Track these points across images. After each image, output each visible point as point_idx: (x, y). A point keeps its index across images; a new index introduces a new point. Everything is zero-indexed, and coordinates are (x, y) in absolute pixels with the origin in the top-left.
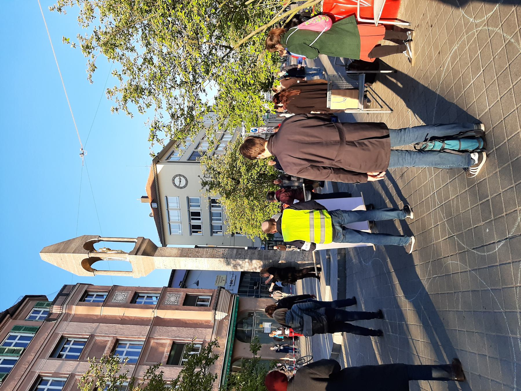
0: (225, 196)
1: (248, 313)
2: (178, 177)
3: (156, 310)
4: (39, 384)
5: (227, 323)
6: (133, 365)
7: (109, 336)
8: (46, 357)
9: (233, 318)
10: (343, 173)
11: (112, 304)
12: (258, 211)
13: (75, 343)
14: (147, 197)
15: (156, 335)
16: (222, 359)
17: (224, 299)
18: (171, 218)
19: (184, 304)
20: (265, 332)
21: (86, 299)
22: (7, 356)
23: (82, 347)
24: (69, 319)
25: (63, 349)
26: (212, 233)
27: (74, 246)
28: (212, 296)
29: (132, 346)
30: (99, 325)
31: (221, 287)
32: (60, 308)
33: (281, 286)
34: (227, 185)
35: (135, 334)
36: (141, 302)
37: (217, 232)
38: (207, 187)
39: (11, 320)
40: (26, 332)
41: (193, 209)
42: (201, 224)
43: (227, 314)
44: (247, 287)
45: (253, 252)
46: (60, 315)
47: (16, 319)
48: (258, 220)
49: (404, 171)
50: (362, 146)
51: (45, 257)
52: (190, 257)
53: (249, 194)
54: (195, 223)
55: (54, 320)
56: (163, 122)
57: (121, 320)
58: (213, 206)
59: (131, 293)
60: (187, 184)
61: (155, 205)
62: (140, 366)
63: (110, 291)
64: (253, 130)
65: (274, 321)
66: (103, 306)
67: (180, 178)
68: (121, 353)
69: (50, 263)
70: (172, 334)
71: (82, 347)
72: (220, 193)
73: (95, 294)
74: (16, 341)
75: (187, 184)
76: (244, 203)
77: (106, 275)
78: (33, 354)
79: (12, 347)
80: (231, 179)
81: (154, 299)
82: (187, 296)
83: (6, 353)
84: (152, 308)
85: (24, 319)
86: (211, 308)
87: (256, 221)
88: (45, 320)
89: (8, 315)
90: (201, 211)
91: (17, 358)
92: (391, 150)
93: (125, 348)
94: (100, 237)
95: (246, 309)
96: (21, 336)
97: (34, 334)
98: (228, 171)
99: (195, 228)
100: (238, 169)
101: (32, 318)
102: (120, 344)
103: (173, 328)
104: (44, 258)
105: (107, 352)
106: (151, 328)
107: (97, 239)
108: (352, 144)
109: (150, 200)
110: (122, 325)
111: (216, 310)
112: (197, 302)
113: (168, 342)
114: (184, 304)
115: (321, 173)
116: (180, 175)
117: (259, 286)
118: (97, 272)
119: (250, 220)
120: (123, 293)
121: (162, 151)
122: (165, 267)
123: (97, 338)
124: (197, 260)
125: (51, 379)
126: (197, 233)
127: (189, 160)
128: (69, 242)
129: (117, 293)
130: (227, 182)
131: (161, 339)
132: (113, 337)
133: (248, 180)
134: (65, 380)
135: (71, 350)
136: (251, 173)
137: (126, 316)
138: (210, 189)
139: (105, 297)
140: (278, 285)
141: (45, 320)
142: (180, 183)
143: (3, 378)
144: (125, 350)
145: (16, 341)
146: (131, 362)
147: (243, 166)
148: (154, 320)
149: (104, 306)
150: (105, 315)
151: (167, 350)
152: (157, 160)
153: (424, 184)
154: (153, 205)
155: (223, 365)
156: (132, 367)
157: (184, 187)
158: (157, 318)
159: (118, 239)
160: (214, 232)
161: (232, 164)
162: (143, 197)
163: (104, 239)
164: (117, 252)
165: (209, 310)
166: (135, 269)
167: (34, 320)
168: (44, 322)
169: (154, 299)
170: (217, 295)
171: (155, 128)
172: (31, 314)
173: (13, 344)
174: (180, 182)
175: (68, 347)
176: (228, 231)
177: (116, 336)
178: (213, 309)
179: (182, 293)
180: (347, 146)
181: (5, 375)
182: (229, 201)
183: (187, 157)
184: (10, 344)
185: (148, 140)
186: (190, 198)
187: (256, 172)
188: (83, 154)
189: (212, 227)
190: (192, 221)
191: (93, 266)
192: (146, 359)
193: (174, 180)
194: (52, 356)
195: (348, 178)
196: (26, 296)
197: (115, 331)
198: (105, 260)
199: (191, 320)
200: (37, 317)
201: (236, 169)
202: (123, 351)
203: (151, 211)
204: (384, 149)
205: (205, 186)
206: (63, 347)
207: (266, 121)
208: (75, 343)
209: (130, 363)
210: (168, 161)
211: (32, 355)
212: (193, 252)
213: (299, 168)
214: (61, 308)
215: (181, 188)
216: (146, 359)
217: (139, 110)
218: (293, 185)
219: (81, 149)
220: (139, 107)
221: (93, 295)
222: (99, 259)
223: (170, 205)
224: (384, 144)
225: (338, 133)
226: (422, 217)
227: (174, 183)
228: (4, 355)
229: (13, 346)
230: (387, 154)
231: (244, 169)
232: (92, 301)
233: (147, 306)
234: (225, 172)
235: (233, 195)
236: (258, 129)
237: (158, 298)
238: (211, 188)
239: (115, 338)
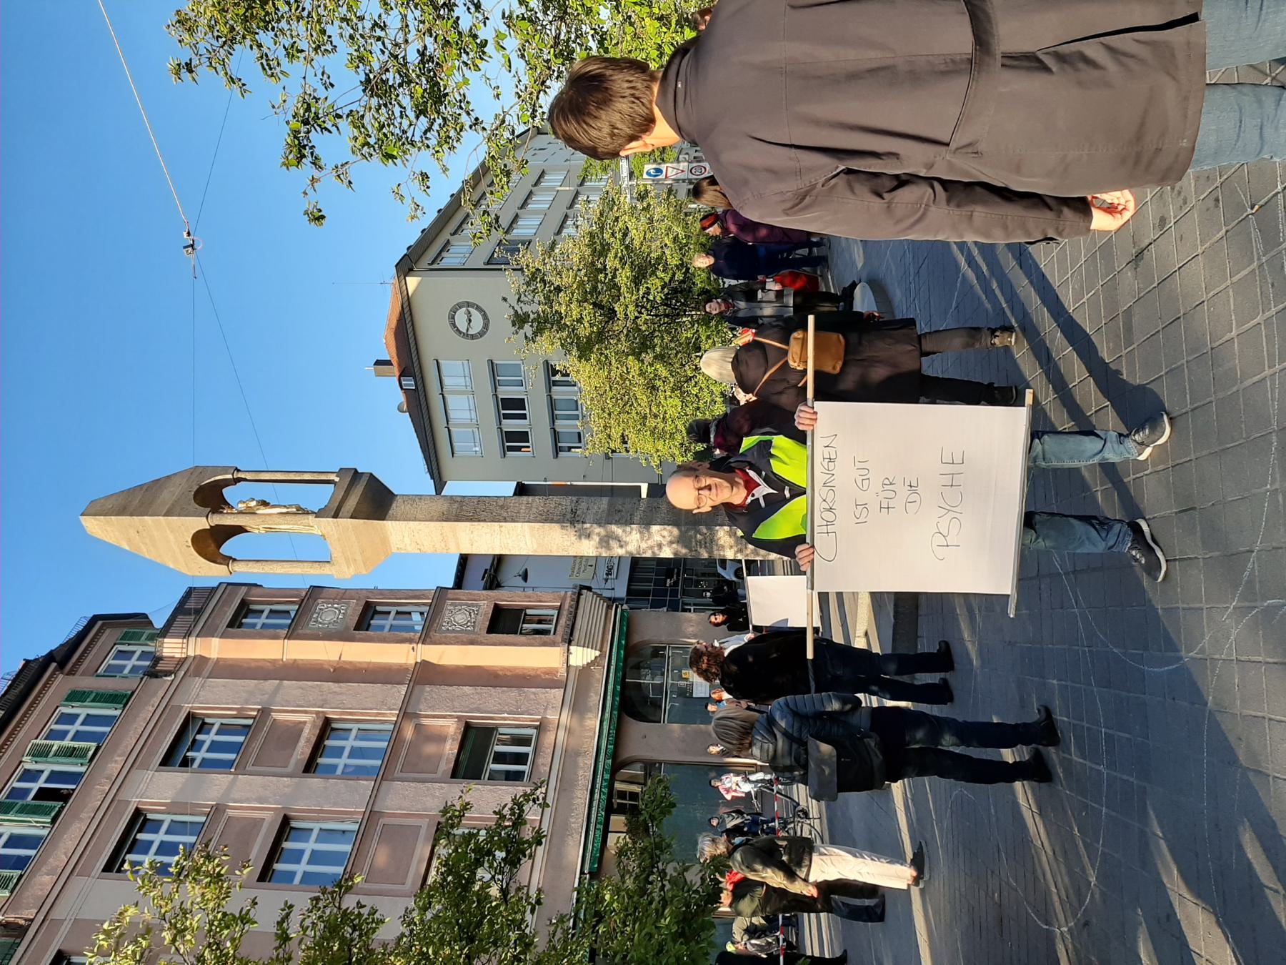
0: (575, 352)
1: (651, 649)
2: (464, 309)
3: (420, 645)
4: (140, 831)
5: (600, 674)
6: (366, 780)
7: (306, 712)
8: (152, 766)
9: (613, 662)
10: (983, 202)
11: (308, 632)
12: (668, 393)
13: (224, 730)
14: (388, 363)
15: (421, 707)
16: (589, 763)
17: (592, 614)
18: (452, 415)
19: (492, 629)
20: (694, 696)
21: (244, 620)
22: (58, 763)
23: (240, 739)
24: (206, 672)
25: (195, 745)
26: (557, 450)
27: (167, 496)
28: (560, 609)
29: (364, 734)
30: (277, 689)
31: (582, 587)
32: (180, 646)
33: (734, 579)
34: (580, 320)
35: (371, 706)
36: (382, 627)
37: (570, 449)
38: (528, 329)
39: (61, 676)
40: (104, 705)
41: (507, 392)
42: (529, 430)
43: (598, 653)
44: (649, 581)
45: (655, 504)
46: (182, 661)
47: (74, 674)
48: (668, 416)
49: (1147, 242)
50: (1077, 70)
51: (95, 526)
52: (485, 521)
53: (642, 345)
54: (512, 425)
55: (168, 673)
56: (329, 102)
57: (334, 671)
58: (555, 383)
59: (357, 604)
60: (486, 327)
61: (409, 383)
62: (384, 782)
63: (303, 600)
64: (652, 172)
65: (710, 735)
66: (288, 637)
67: (469, 313)
68: (338, 752)
69: (111, 542)
70: (463, 704)
71: (240, 739)
72: (562, 345)
73: (267, 608)
74: (77, 726)
75: (486, 327)
76: (628, 373)
77: (260, 571)
78: (121, 760)
79: (67, 743)
80: (591, 307)
81: (416, 617)
82: (498, 610)
83: (55, 755)
84: (410, 641)
85: (95, 673)
86: (558, 638)
87: (664, 418)
88: (145, 675)
89: (54, 665)
90: (525, 397)
91: (83, 769)
92: (1207, 84)
93: (347, 739)
94: (239, 471)
95: (646, 638)
96: (88, 715)
97: (120, 708)
98: (581, 284)
99: (515, 440)
100: (610, 276)
101: (113, 672)
102: (333, 729)
103: (466, 689)
104: (94, 531)
105: (303, 749)
106: (410, 690)
107: (230, 476)
108: (1030, 62)
109: (395, 369)
110: (336, 685)
111: (570, 643)
112: (523, 623)
113: (452, 728)
114: (492, 629)
115: (890, 203)
116: (468, 302)
117: (678, 580)
118: (235, 564)
119: (645, 417)
120: (336, 606)
121: (419, 242)
122: (418, 547)
123: (275, 715)
124: (503, 529)
125: (167, 819)
126: (520, 451)
127: (488, 264)
128: (158, 484)
129: (321, 605)
130: (581, 315)
131: (434, 717)
132: (317, 713)
133: (637, 306)
134: (203, 819)
135: (215, 747)
136: (647, 288)
137: (345, 662)
138: (535, 334)
139: (293, 614)
140: (727, 578)
141: (145, 675)
142: (469, 324)
143: (53, 814)
144: (349, 744)
145: (77, 726)
146: (359, 773)
147: (623, 269)
148: (416, 669)
149: (288, 637)
150: (295, 660)
151: (450, 749)
152: (406, 266)
153: (1235, 279)
154: (403, 383)
155: (591, 779)
156: (367, 785)
157: (481, 334)
158: (424, 665)
159: (287, 474)
160: (561, 449)
161: (593, 263)
162: (378, 363)
163: (248, 476)
164: (284, 510)
165: (553, 644)
166: (336, 554)
167: (118, 675)
168: (142, 679)
169: (416, 617)
170: (571, 607)
171: (306, 122)
172: (110, 661)
173: (70, 736)
174: (470, 320)
175: (207, 739)
176: (589, 447)
177: (323, 712)
178: (563, 641)
179: (485, 602)
180: (1008, 75)
181: (57, 809)
182: (588, 367)
183: (485, 257)
184: (62, 735)
185: (284, 164)
186: (495, 362)
187: (659, 284)
188: (192, 246)
189: (556, 436)
190: (504, 421)
191: (226, 549)
192: (399, 766)
193: (453, 318)
194: (166, 762)
195: (1009, 222)
196: (94, 616)
197: (320, 698)
198: (257, 531)
199: (508, 669)
200: (124, 667)
201: (605, 278)
202: (343, 748)
203: (401, 398)
204: (1174, 78)
205: (521, 327)
206: (194, 741)
207: (687, 154)
208: (224, 730)
209: (360, 777)
210: (435, 266)
211: (116, 761)
212: (492, 507)
213: (793, 186)
214: (185, 646)
215: (473, 337)
216: (399, 766)
217: (264, 69)
218: (759, 313)
219: (185, 234)
220: (262, 57)
221: (262, 612)
222: (240, 530)
223: (446, 381)
224: (1173, 55)
225: (966, 19)
226: (1221, 395)
227: (454, 325)
228: (49, 759)
229: (72, 740)
230: (1186, 99)
231: (628, 278)
232: (258, 627)
233: (398, 636)
234: (575, 286)
235: (598, 349)
236: (663, 167)
237: (426, 614)
238: (539, 331)
239: (321, 715)
